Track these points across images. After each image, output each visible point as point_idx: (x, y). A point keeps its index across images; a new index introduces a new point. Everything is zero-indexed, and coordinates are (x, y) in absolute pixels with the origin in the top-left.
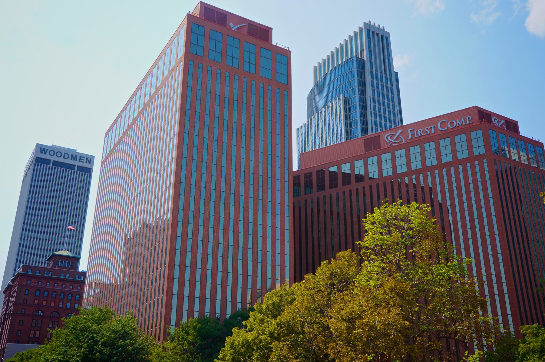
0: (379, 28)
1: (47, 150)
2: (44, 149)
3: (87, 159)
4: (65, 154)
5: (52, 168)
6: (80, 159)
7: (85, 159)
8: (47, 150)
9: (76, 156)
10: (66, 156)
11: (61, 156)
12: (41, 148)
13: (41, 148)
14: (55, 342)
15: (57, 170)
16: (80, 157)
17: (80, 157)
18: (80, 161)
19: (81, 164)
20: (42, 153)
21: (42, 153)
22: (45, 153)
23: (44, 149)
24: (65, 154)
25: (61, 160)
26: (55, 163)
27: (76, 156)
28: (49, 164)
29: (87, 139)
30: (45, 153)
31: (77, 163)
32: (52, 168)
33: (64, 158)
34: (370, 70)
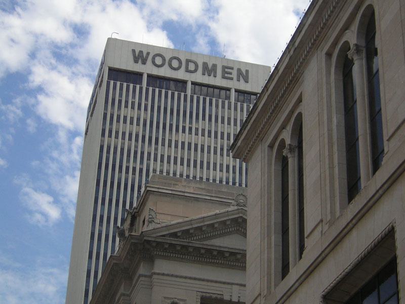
0: (225, 236)
1: (148, 54)
2: (141, 52)
3: (239, 70)
4: (188, 61)
5: (147, 90)
6: (224, 72)
7: (235, 73)
8: (148, 54)
9: (215, 66)
10: (192, 67)
11: (196, 71)
12: (134, 51)
13: (134, 51)
14: (289, 156)
15: (121, 89)
16: (224, 67)
17: (224, 67)
18: (224, 77)
19: (156, 72)
20: (136, 61)
21: (136, 61)
22: (144, 63)
23: (141, 52)
24: (188, 61)
25: (165, 72)
26: (154, 80)
27: (215, 66)
28: (140, 83)
29: (355, 42)
30: (144, 63)
31: (148, 69)
32: (147, 90)
33: (187, 71)
34: (179, 278)
